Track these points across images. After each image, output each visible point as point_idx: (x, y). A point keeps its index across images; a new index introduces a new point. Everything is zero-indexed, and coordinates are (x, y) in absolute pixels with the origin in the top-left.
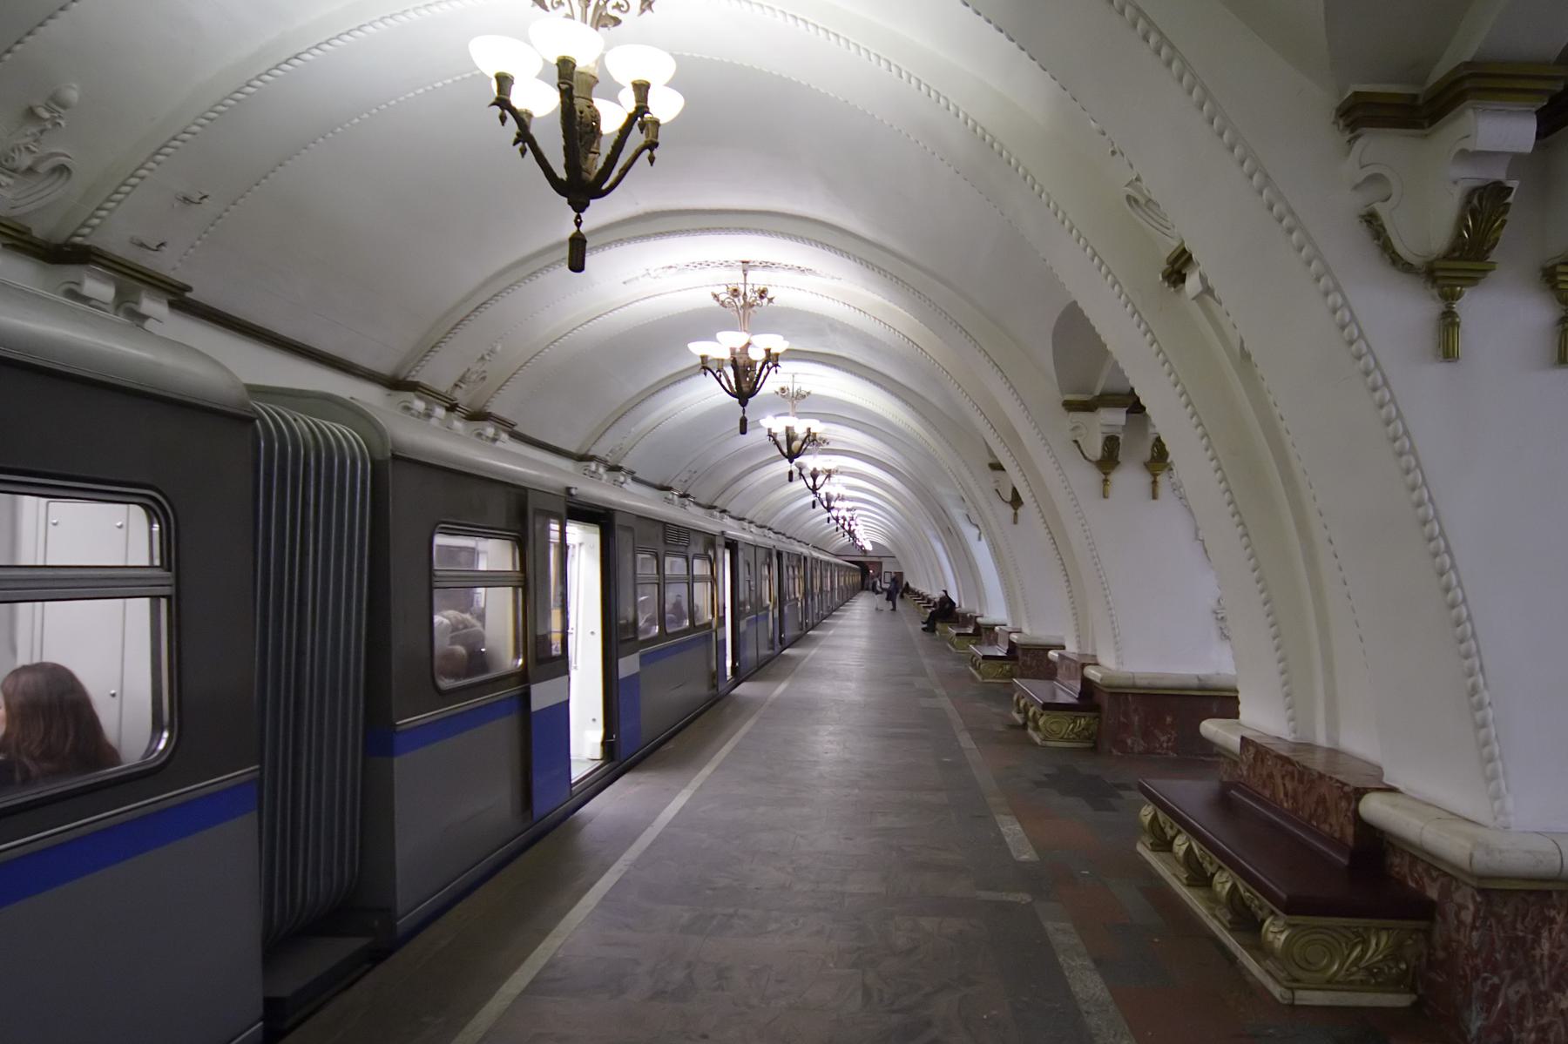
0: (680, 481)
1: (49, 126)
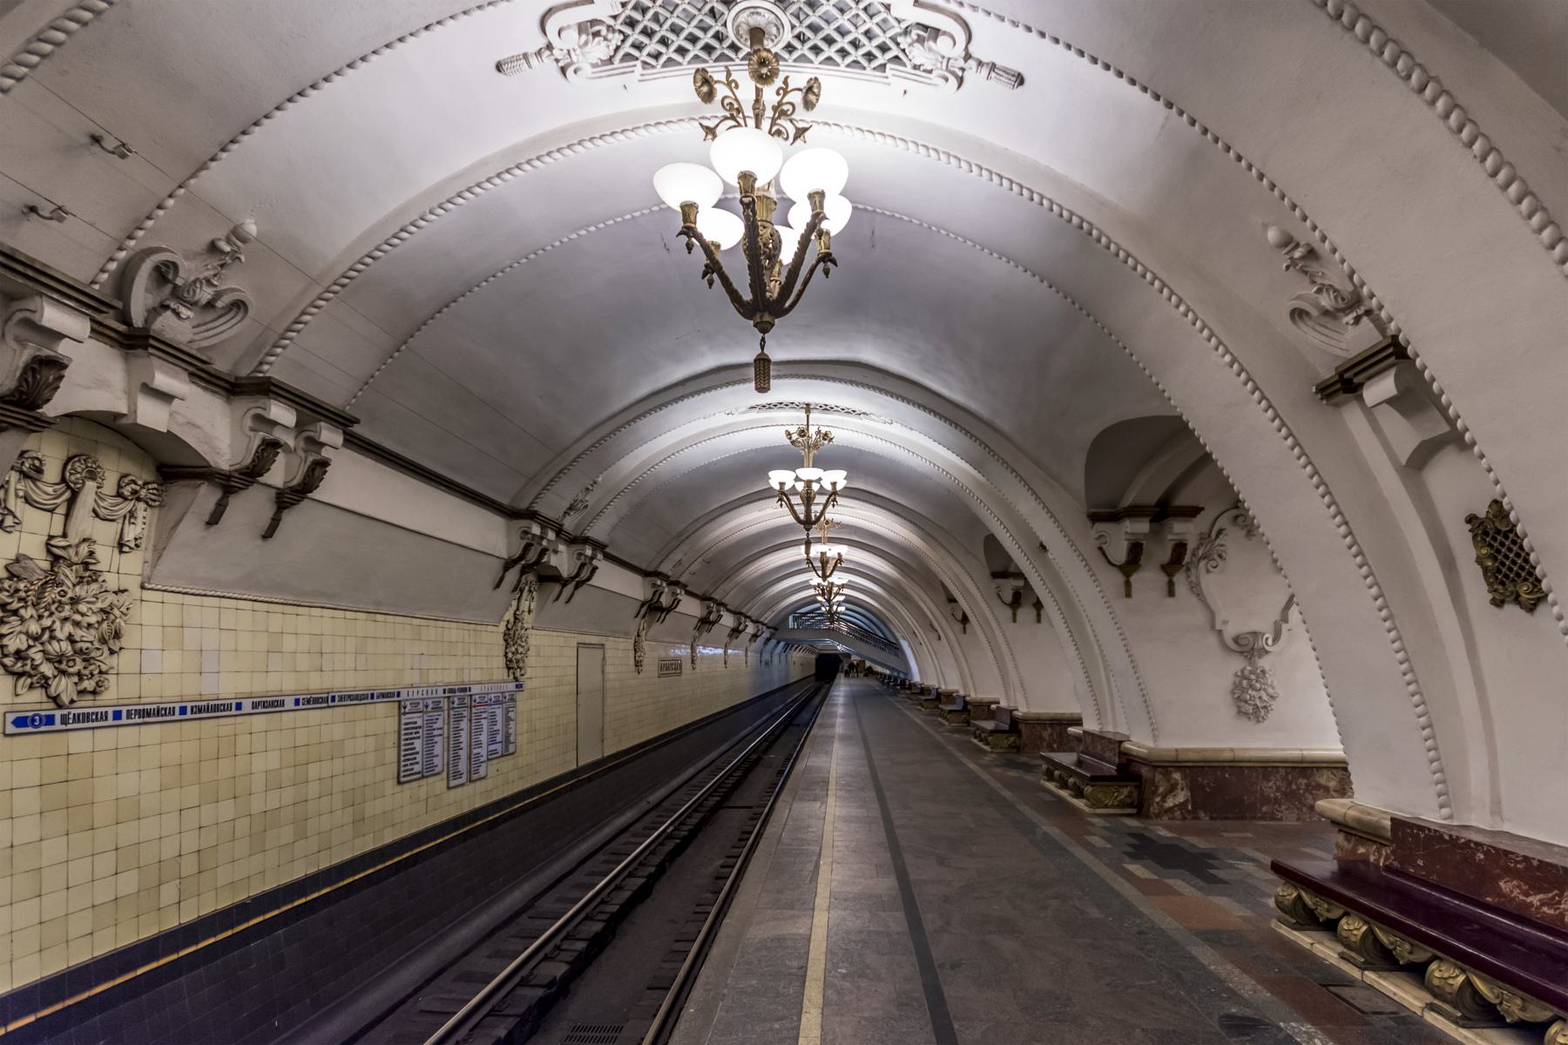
1: (228, 260)
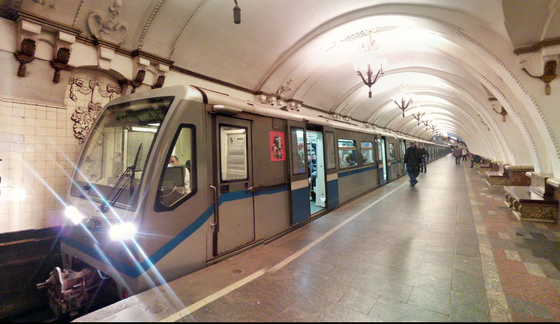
0: (351, 112)
